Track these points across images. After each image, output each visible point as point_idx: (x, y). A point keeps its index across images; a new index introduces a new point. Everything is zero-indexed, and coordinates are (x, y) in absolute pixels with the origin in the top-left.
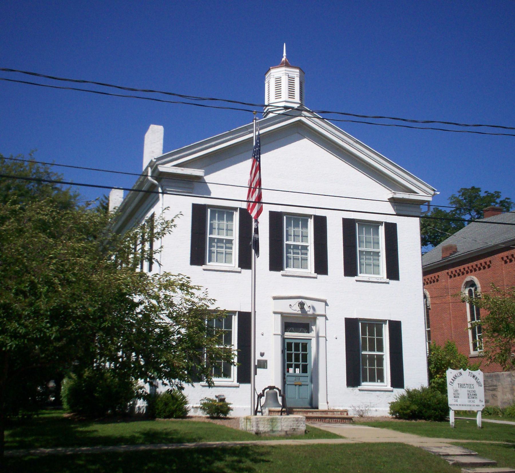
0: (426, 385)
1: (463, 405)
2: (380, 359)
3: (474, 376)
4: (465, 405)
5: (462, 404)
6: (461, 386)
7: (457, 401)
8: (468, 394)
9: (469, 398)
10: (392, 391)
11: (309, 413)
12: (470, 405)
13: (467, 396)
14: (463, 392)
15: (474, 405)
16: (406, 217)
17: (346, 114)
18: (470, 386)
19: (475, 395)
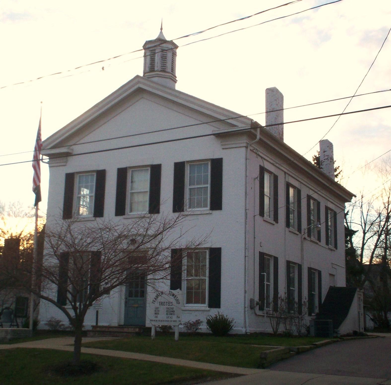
0: (345, 286)
1: (161, 321)
2: (208, 175)
3: (173, 295)
4: (164, 321)
5: (161, 319)
6: (162, 304)
7: (157, 317)
8: (167, 311)
9: (167, 314)
10: (209, 311)
11: (316, 194)
12: (168, 321)
13: (165, 313)
14: (162, 309)
15: (171, 321)
16: (135, 165)
17: (101, 61)
18: (170, 303)
19: (174, 311)
